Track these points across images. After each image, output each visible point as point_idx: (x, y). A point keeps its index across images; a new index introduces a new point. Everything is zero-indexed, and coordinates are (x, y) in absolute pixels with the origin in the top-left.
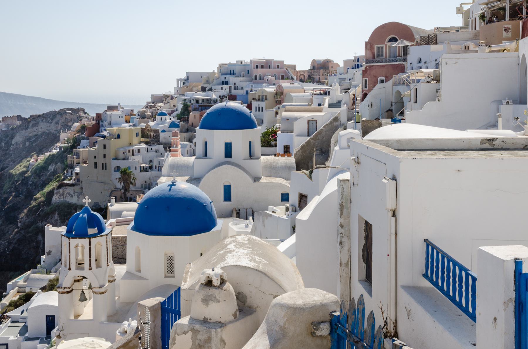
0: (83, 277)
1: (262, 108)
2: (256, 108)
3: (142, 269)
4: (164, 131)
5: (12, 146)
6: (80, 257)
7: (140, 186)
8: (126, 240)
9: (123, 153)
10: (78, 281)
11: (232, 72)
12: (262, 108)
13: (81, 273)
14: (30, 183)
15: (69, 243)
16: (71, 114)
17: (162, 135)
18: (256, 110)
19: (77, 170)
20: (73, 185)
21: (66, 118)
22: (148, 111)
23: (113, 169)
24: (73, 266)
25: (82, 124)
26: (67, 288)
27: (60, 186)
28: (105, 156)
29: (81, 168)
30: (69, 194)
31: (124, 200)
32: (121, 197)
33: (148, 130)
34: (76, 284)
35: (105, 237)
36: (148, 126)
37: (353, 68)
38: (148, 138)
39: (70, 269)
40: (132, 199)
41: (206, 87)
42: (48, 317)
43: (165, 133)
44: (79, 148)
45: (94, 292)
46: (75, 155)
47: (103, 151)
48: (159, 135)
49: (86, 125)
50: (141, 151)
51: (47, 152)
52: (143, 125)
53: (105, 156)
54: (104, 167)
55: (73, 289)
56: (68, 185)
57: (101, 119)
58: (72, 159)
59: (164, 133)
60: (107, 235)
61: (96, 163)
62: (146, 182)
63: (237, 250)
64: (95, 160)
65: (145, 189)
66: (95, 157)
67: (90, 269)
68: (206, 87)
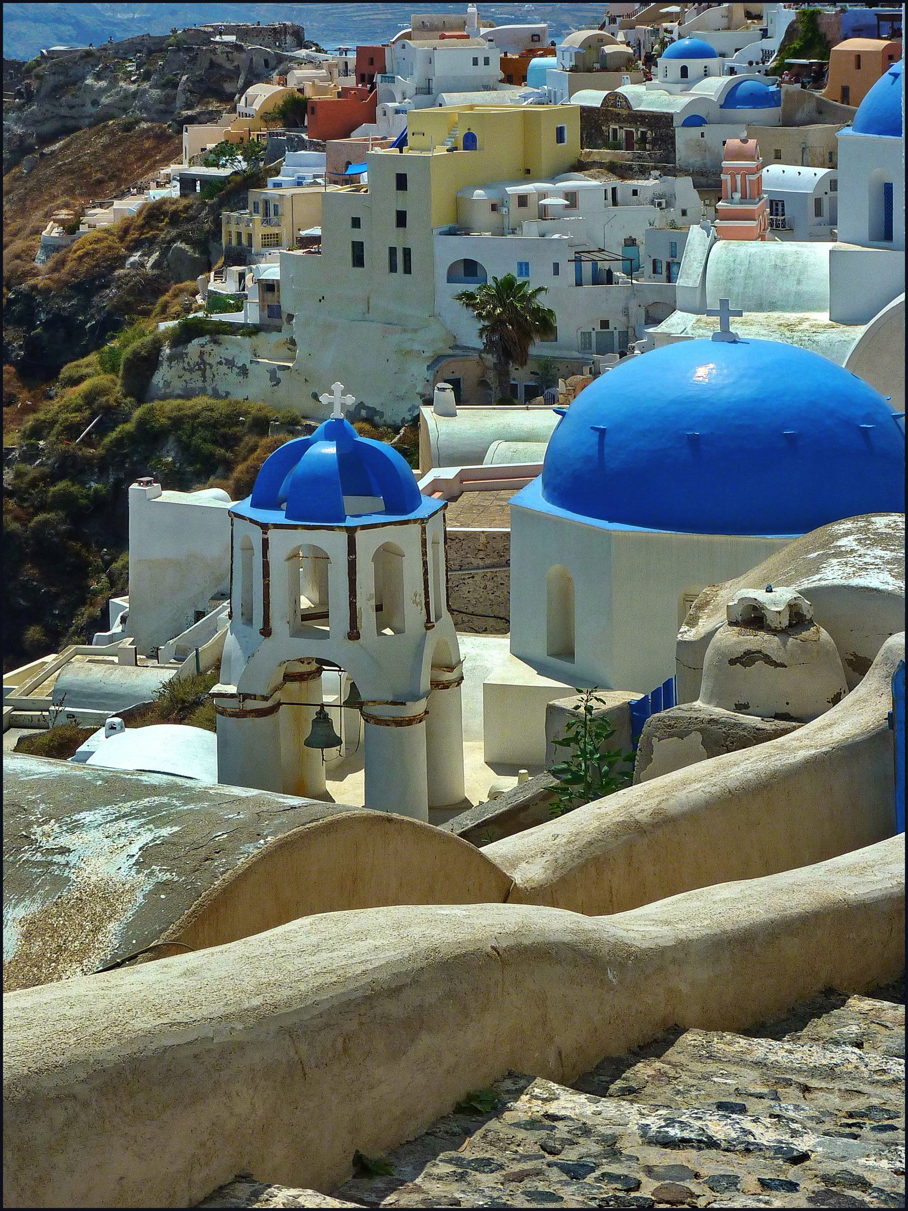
0: (322, 662)
3: (579, 651)
4: (694, 121)
7: (577, 340)
8: (507, 549)
9: (494, 208)
10: (301, 677)
13: (312, 648)
14: (43, 316)
15: (265, 543)
16: (238, 48)
17: (683, 137)
19: (270, 270)
20: (252, 331)
22: (620, 37)
23: (442, 272)
24: (278, 624)
25: (292, 84)
26: (254, 697)
27: (189, 331)
28: (401, 219)
29: (284, 261)
30: (230, 363)
31: (496, 392)
32: (483, 383)
33: (617, 118)
34: (293, 686)
35: (417, 527)
36: (614, 100)
38: (617, 147)
39: (266, 632)
40: (536, 392)
43: (704, 129)
44: (278, 185)
45: (368, 718)
46: (256, 211)
47: (395, 201)
48: (673, 137)
49: (309, 93)
50: (581, 200)
51: (122, 196)
52: (592, 98)
53: (401, 219)
54: (401, 261)
55: (280, 704)
56: (232, 329)
58: (242, 228)
59: (695, 132)
60: (423, 521)
62: (605, 324)
63: (862, 551)
64: (357, 235)
65: (601, 351)
66: (356, 223)
67: (354, 634)
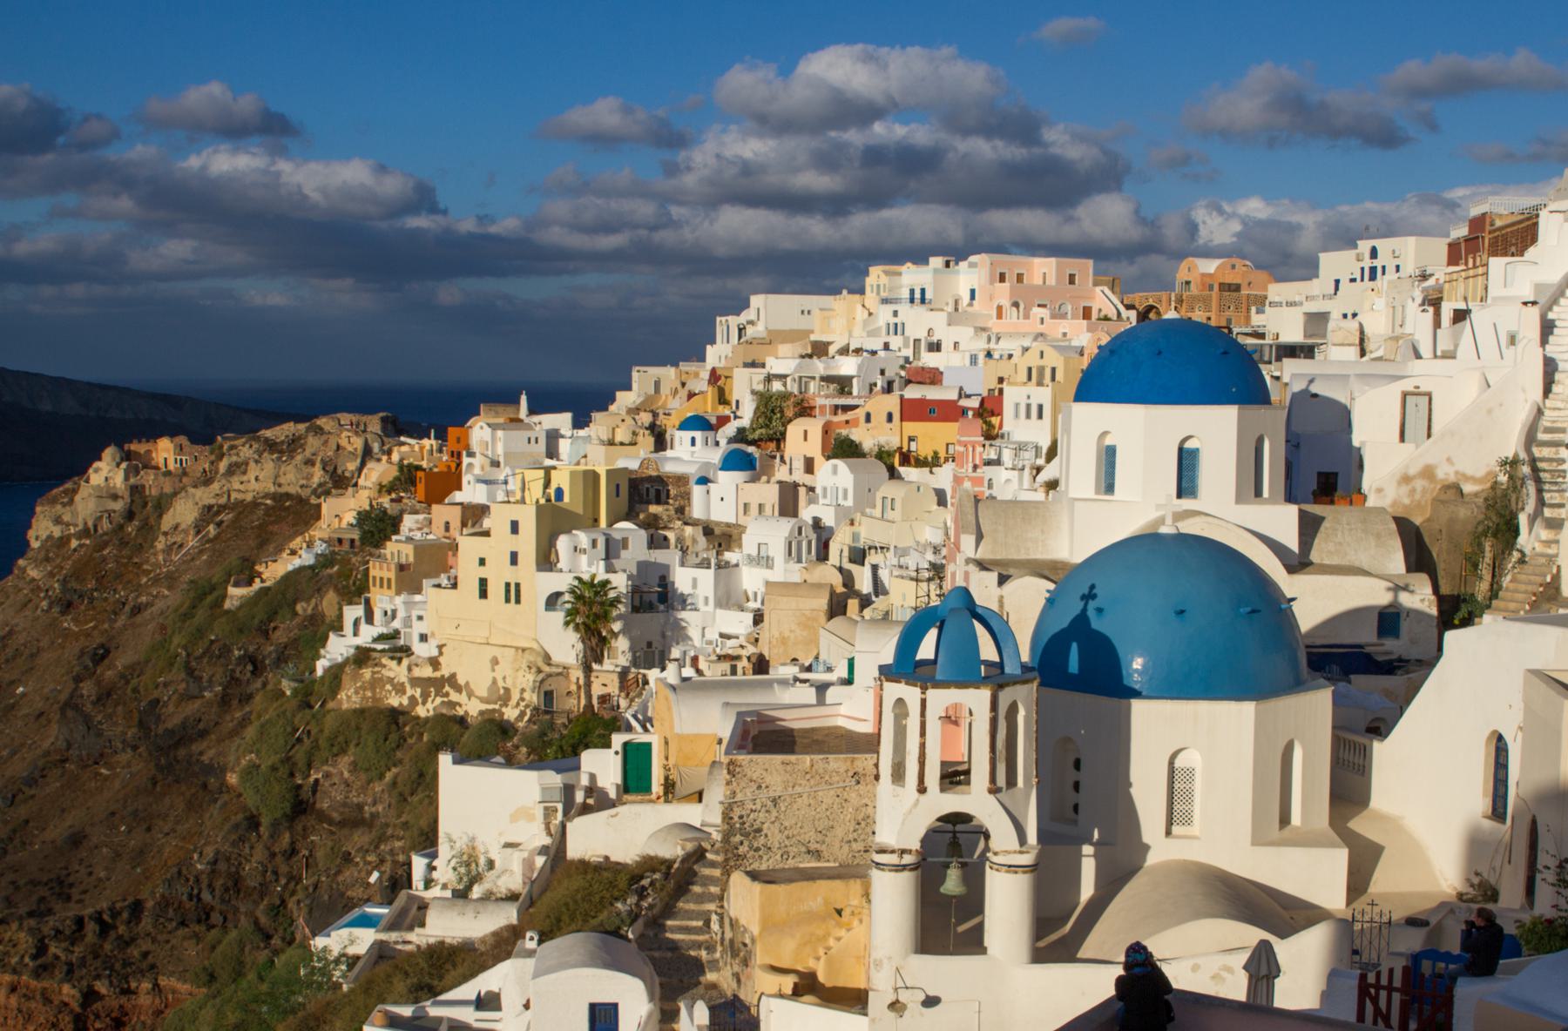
1: (1040, 407)
2: (1017, 405)
5: (162, 538)
6: (960, 754)
11: (918, 295)
12: (1040, 407)
18: (1017, 416)
21: (338, 447)
37: (1353, 280)
41: (829, 343)
42: (593, 1007)
57: (467, 447)
61: (483, 583)
62: (649, 645)
64: (483, 572)
66: (482, 562)
68: (829, 343)
